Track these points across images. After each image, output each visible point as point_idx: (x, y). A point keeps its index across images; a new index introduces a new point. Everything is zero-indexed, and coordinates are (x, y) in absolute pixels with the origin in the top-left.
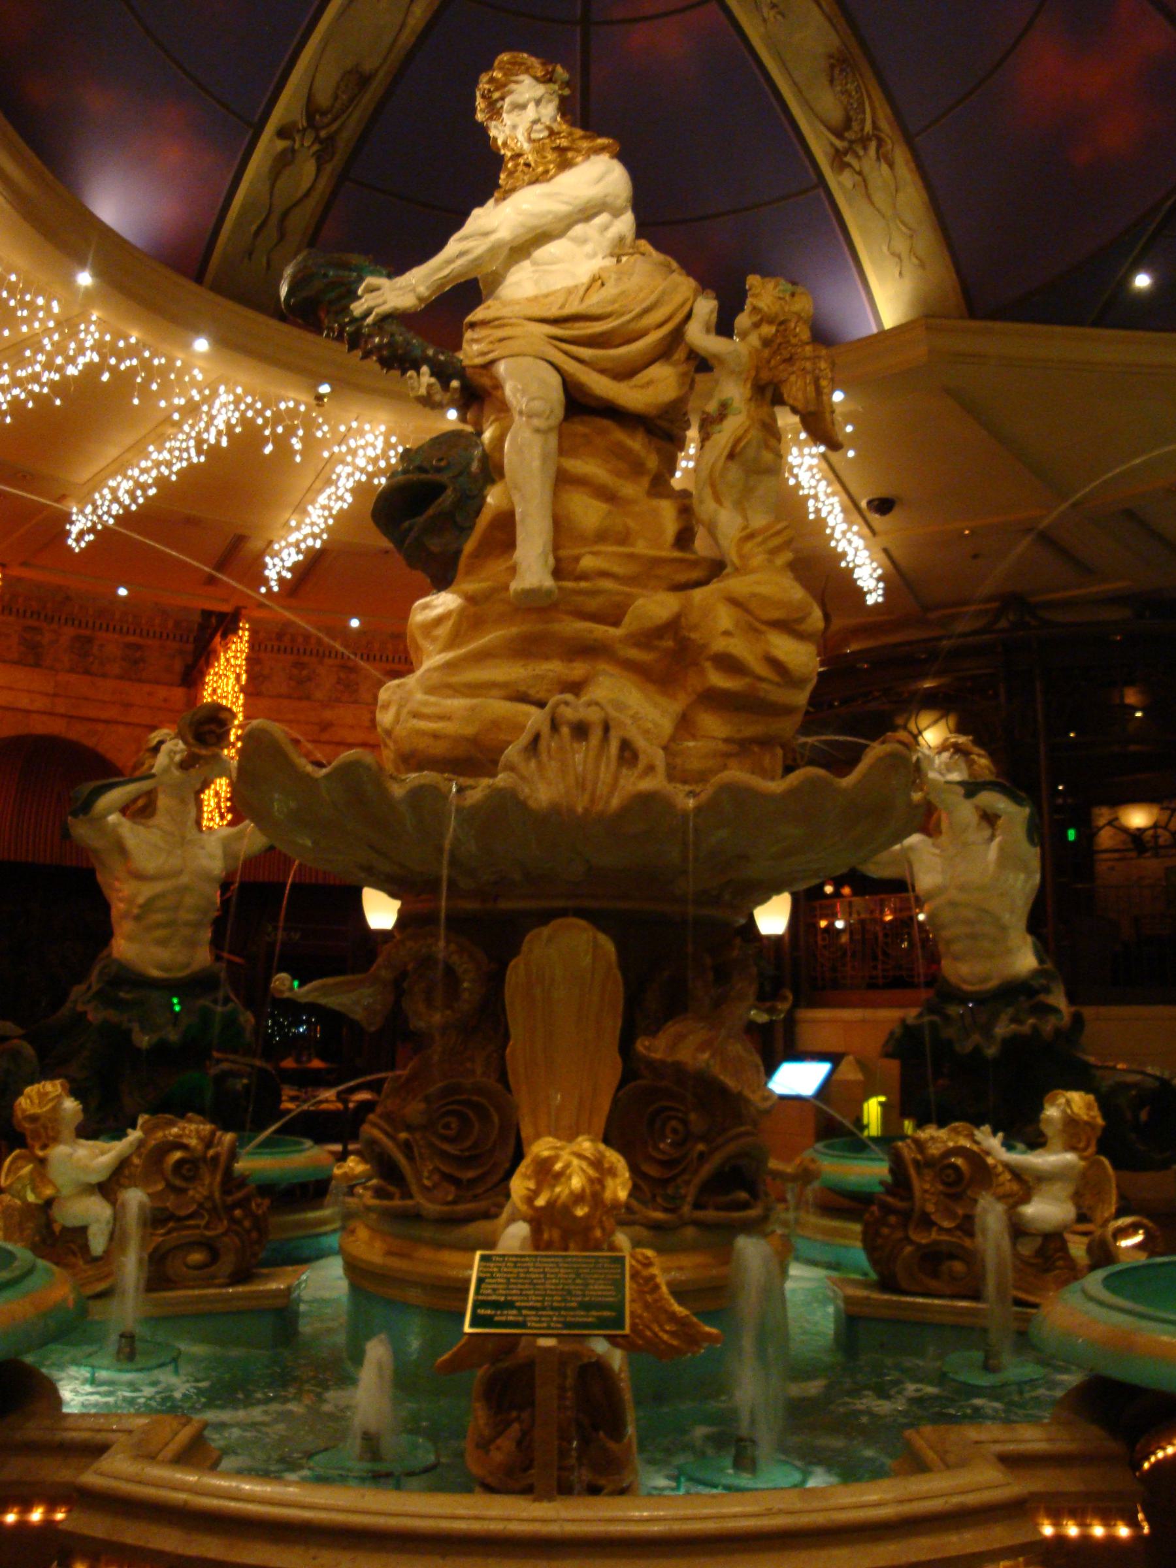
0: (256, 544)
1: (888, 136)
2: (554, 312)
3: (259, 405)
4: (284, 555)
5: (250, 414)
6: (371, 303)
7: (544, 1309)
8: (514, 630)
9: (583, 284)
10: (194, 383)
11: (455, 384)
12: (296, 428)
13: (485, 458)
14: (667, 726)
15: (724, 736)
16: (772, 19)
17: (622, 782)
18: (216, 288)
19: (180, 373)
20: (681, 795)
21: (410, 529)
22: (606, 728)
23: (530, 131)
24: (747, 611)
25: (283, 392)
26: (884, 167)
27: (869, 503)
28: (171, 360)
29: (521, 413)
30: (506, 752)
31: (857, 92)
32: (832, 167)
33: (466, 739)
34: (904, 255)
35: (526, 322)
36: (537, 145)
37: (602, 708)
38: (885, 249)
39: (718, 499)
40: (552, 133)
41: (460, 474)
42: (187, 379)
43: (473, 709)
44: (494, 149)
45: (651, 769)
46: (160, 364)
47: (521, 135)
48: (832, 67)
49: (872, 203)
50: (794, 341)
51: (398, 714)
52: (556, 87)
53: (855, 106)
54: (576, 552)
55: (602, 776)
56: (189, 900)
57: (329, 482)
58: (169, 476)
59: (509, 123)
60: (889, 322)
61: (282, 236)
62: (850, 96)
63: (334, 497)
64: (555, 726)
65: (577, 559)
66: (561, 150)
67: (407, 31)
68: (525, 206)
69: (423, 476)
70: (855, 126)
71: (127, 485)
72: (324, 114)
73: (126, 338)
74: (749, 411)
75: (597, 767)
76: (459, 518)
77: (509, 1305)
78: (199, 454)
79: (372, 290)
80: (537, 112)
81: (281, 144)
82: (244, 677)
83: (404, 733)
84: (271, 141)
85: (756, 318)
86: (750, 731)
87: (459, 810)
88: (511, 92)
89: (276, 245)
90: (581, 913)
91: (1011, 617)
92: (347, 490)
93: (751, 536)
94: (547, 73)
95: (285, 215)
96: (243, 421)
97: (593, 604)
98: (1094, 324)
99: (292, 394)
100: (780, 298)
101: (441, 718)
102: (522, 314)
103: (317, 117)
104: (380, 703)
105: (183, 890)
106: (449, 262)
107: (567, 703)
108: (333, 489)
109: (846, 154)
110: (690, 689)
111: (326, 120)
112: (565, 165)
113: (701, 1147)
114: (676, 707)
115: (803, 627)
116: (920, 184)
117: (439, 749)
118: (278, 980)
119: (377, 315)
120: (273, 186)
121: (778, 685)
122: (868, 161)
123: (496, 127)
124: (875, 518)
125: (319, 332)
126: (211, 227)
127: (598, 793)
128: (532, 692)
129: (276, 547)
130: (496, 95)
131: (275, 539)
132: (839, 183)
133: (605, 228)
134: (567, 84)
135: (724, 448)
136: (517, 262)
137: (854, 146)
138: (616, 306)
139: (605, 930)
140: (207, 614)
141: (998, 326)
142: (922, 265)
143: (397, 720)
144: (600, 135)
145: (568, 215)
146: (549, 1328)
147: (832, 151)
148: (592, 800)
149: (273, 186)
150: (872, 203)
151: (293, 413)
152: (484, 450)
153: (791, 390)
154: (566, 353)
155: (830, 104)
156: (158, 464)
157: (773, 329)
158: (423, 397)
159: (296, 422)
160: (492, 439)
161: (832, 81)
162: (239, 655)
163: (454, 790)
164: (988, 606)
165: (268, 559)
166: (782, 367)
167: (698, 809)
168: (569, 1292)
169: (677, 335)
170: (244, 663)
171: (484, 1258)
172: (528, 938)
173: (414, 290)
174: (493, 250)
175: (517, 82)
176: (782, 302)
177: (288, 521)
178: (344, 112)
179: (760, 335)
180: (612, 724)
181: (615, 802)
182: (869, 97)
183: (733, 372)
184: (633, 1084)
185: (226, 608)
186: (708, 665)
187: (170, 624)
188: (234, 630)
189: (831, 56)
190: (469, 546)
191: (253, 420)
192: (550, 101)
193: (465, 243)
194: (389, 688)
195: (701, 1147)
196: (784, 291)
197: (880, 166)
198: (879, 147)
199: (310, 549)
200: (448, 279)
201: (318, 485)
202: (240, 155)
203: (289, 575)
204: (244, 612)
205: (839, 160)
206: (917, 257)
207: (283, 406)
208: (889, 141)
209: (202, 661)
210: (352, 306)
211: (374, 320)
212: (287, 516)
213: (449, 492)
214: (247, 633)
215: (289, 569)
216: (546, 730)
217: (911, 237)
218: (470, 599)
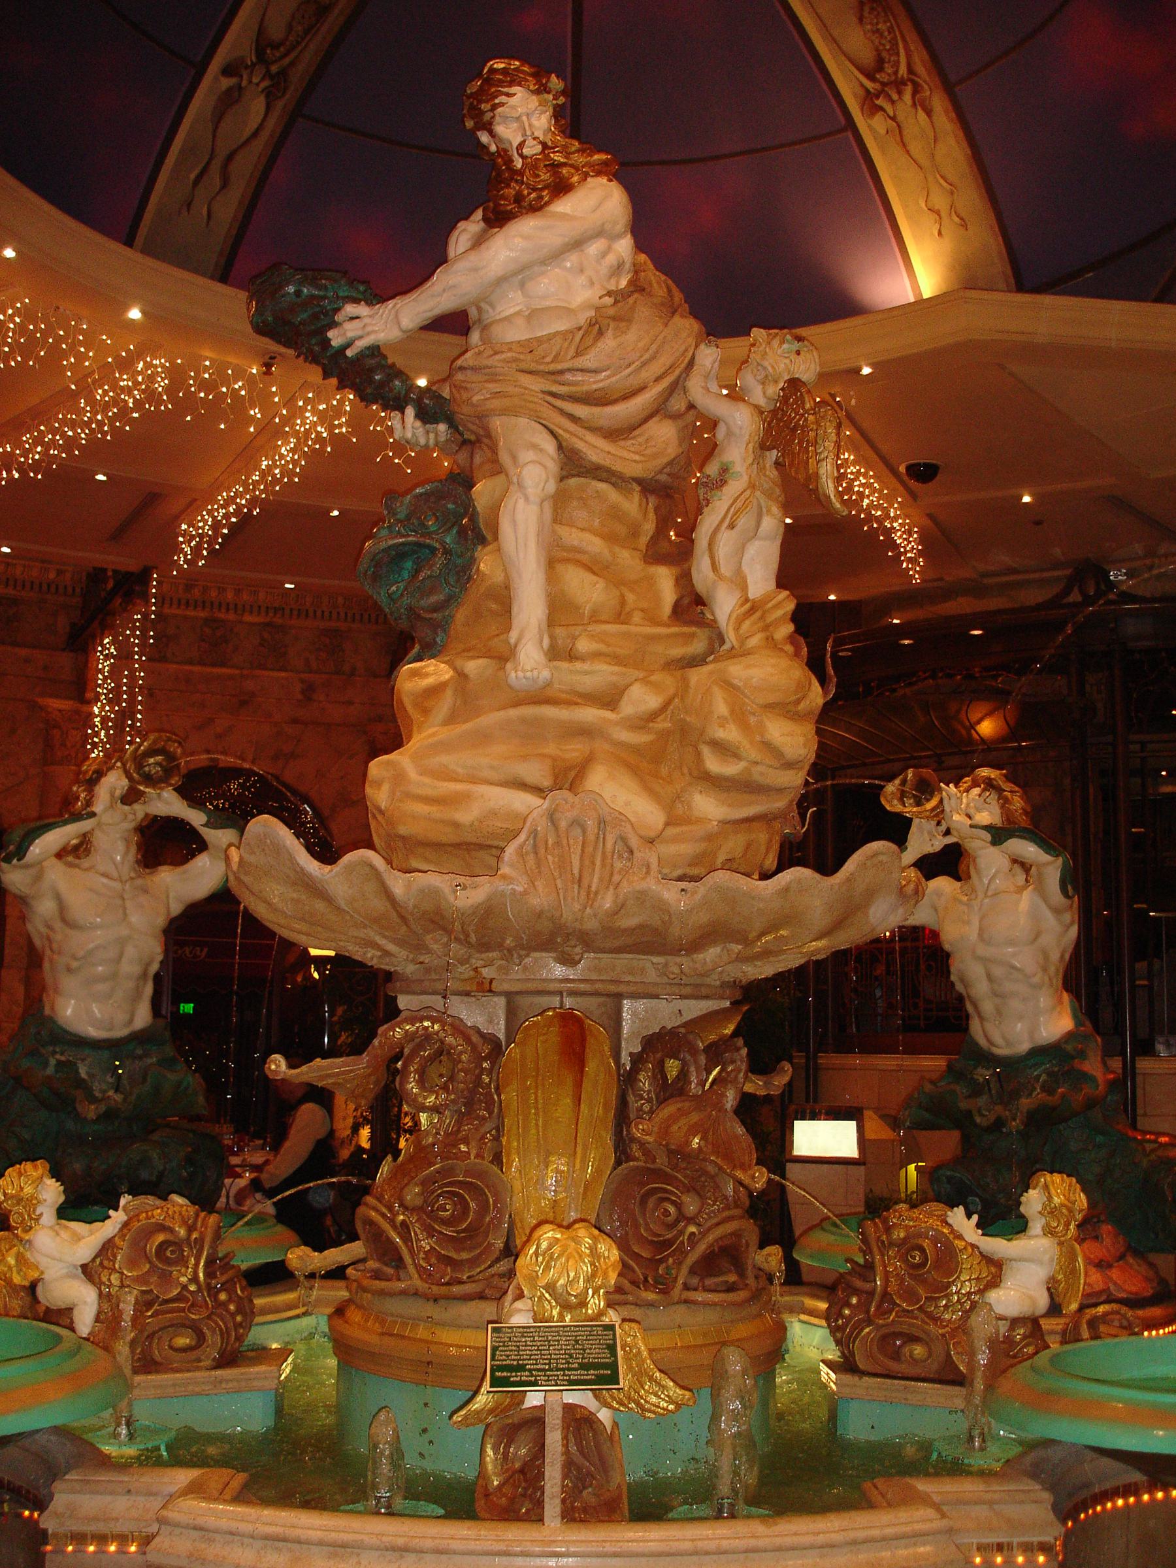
1: (925, 82)
7: (550, 1370)
9: (580, 329)
26: (921, 115)
27: (908, 468)
31: (890, 33)
32: (862, 110)
49: (908, 152)
52: (550, 97)
61: (225, 183)
62: (882, 36)
70: (889, 69)
72: (275, 46)
77: (521, 1368)
81: (226, 83)
84: (216, 79)
88: (502, 104)
89: (218, 193)
95: (230, 158)
98: (1156, 301)
109: (878, 98)
113: (692, 1229)
116: (961, 134)
120: (216, 128)
132: (869, 126)
134: (563, 93)
140: (97, 575)
142: (964, 225)
144: (599, 151)
146: (557, 1385)
147: (861, 92)
149: (216, 128)
150: (908, 152)
154: (562, 412)
155: (859, 42)
161: (861, 19)
164: (1056, 573)
168: (571, 1356)
171: (494, 1330)
175: (508, 95)
176: (787, 361)
178: (298, 43)
184: (624, 1165)
195: (692, 1229)
198: (915, 92)
205: (870, 103)
208: (926, 86)
217: (952, 193)
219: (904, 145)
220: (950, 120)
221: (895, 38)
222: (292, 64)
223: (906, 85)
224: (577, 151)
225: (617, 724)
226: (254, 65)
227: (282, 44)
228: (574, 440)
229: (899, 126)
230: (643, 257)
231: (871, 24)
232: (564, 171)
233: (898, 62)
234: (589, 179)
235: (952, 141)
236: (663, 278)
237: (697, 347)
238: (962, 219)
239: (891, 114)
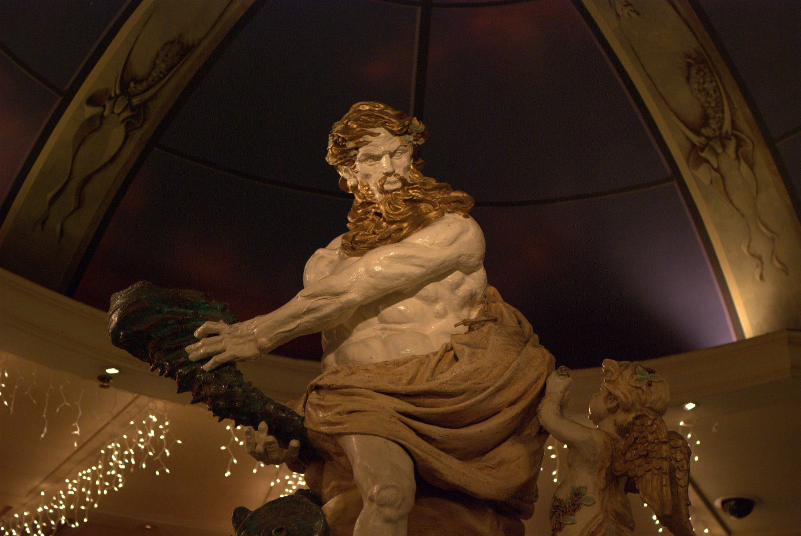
1: (749, 138)
6: (210, 349)
9: (435, 354)
11: (294, 443)
26: (744, 168)
27: (724, 503)
29: (371, 500)
31: (715, 92)
32: (688, 161)
34: (765, 259)
35: (375, 394)
38: (745, 250)
48: (689, 65)
49: (731, 201)
52: (411, 138)
53: (713, 105)
60: (748, 332)
61: (80, 202)
62: (708, 94)
66: (413, 202)
68: (378, 269)
70: (713, 124)
72: (138, 82)
80: (392, 164)
81: (90, 111)
85: (612, 405)
88: (366, 143)
89: (73, 212)
94: (404, 127)
95: (87, 180)
102: (371, 385)
103: (132, 85)
109: (702, 150)
111: (140, 88)
112: (420, 222)
119: (215, 363)
123: (346, 171)
124: (731, 521)
125: (143, 358)
130: (350, 145)
134: (423, 134)
136: (365, 319)
137: (711, 143)
142: (785, 270)
145: (422, 276)
150: (731, 201)
157: (631, 417)
158: (259, 454)
161: (688, 79)
166: (638, 462)
169: (532, 411)
173: (255, 340)
174: (342, 309)
175: (372, 134)
176: (640, 392)
177: (35, 492)
178: (161, 79)
179: (615, 421)
182: (729, 98)
193: (313, 300)
196: (640, 380)
197: (740, 164)
205: (695, 154)
206: (779, 262)
208: (749, 141)
217: (773, 240)
219: (727, 194)
223: (730, 139)
224: (435, 188)
226: (117, 96)
228: (431, 459)
229: (723, 177)
230: (492, 290)
231: (699, 83)
232: (423, 206)
233: (723, 118)
234: (446, 215)
236: (513, 309)
237: (548, 375)
238: (782, 264)
239: (716, 166)
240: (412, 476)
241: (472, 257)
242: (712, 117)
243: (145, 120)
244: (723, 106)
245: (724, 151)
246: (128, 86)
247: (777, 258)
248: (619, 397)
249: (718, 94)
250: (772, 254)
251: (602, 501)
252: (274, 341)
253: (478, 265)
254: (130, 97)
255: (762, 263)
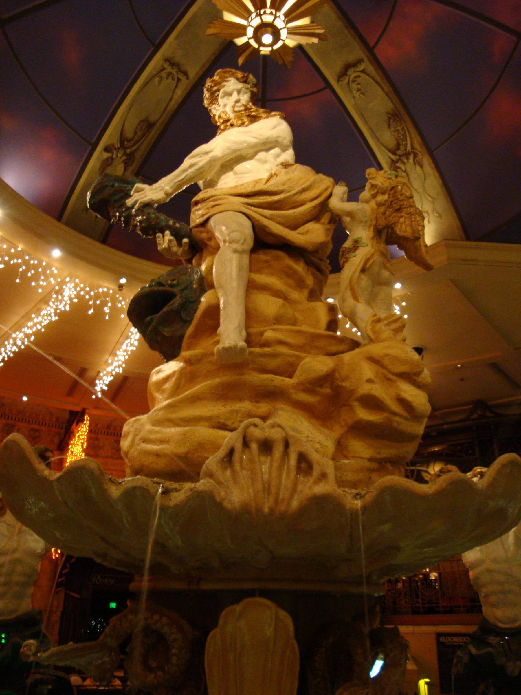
0: (91, 374)
2: (250, 189)
3: (88, 289)
4: (105, 378)
5: (82, 293)
8: (217, 380)
10: (52, 275)
11: (185, 240)
12: (108, 302)
13: (202, 279)
14: (330, 446)
15: (368, 456)
16: (358, 97)
17: (300, 487)
18: (68, 224)
19: (45, 269)
20: (349, 497)
21: (151, 321)
22: (287, 445)
23: (234, 107)
24: (383, 366)
25: (101, 283)
26: (418, 168)
28: (40, 262)
30: (207, 462)
31: (402, 130)
33: (179, 456)
36: (237, 114)
37: (283, 429)
39: (355, 298)
40: (246, 109)
41: (186, 288)
42: (48, 272)
43: (185, 434)
44: (213, 122)
45: (323, 476)
46: (34, 264)
47: (228, 109)
48: (389, 118)
50: (401, 198)
51: (133, 440)
52: (249, 86)
53: (402, 137)
54: (262, 329)
55: (283, 481)
56: (19, 569)
57: (128, 337)
58: (41, 329)
59: (222, 104)
62: (399, 133)
63: (129, 345)
64: (246, 443)
65: (262, 334)
67: (172, 103)
68: (233, 138)
69: (161, 288)
70: (402, 148)
71: (21, 335)
72: (129, 141)
73: (16, 248)
74: (372, 245)
75: (280, 475)
76: (183, 315)
78: (55, 316)
79: (138, 191)
81: (106, 155)
82: (85, 445)
83: (136, 454)
86: (386, 453)
87: (164, 509)
88: (224, 86)
90: (265, 593)
91: (479, 412)
92: (135, 340)
93: (379, 320)
96: (78, 296)
97: (273, 363)
99: (106, 284)
100: (389, 178)
101: (162, 441)
103: (126, 143)
104: (123, 435)
105: (18, 561)
106: (184, 171)
107: (255, 425)
108: (129, 340)
109: (397, 162)
110: (342, 424)
111: (130, 145)
114: (338, 432)
115: (419, 379)
117: (161, 464)
118: (26, 646)
121: (406, 418)
122: (409, 165)
126: (66, 194)
127: (281, 497)
128: (229, 423)
129: (101, 374)
131: (101, 370)
133: (278, 156)
135: (358, 266)
136: (225, 173)
137: (402, 158)
138: (285, 187)
139: (284, 609)
141: (484, 244)
142: (440, 217)
143: (132, 445)
145: (255, 145)
147: (389, 161)
148: (276, 501)
151: (106, 294)
152: (201, 274)
153: (401, 227)
156: (35, 324)
159: (107, 299)
160: (206, 268)
161: (389, 126)
162: (83, 433)
163: (160, 490)
165: (97, 382)
166: (394, 215)
167: (364, 508)
170: (86, 437)
172: (224, 613)
173: (163, 189)
175: (226, 81)
176: (391, 181)
178: (139, 140)
179: (376, 202)
180: (291, 441)
181: (295, 504)
182: (409, 133)
183: (361, 222)
185: (78, 409)
186: (356, 404)
187: (54, 419)
188: (81, 420)
189: (389, 114)
190: (189, 331)
191: (84, 296)
192: (246, 93)
194: (129, 423)
196: (390, 174)
197: (415, 168)
198: (415, 157)
199: (117, 374)
200: (184, 181)
201: (122, 339)
202: (84, 158)
203: (106, 388)
204: (87, 411)
206: (437, 213)
207: (101, 290)
208: (419, 154)
209: (67, 437)
210: (127, 201)
211: (138, 206)
212: (107, 357)
213: (178, 297)
214: (88, 422)
215: (106, 385)
216: (239, 446)
217: (434, 202)
218: (188, 362)
220: (432, 168)
221: (405, 133)
222: (137, 150)
225: (294, 387)
227: (132, 140)
235: (432, 178)
240: (251, 229)
241: (285, 139)
242: (401, 144)
243: (133, 162)
244: (406, 137)
245: (408, 161)
246: (124, 143)
247: (436, 211)
248: (378, 184)
249: (403, 132)
250: (433, 209)
251: (373, 244)
252: (174, 188)
253: (289, 146)
254: (125, 148)
255: (429, 215)
